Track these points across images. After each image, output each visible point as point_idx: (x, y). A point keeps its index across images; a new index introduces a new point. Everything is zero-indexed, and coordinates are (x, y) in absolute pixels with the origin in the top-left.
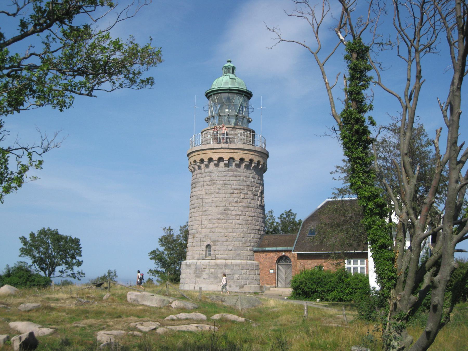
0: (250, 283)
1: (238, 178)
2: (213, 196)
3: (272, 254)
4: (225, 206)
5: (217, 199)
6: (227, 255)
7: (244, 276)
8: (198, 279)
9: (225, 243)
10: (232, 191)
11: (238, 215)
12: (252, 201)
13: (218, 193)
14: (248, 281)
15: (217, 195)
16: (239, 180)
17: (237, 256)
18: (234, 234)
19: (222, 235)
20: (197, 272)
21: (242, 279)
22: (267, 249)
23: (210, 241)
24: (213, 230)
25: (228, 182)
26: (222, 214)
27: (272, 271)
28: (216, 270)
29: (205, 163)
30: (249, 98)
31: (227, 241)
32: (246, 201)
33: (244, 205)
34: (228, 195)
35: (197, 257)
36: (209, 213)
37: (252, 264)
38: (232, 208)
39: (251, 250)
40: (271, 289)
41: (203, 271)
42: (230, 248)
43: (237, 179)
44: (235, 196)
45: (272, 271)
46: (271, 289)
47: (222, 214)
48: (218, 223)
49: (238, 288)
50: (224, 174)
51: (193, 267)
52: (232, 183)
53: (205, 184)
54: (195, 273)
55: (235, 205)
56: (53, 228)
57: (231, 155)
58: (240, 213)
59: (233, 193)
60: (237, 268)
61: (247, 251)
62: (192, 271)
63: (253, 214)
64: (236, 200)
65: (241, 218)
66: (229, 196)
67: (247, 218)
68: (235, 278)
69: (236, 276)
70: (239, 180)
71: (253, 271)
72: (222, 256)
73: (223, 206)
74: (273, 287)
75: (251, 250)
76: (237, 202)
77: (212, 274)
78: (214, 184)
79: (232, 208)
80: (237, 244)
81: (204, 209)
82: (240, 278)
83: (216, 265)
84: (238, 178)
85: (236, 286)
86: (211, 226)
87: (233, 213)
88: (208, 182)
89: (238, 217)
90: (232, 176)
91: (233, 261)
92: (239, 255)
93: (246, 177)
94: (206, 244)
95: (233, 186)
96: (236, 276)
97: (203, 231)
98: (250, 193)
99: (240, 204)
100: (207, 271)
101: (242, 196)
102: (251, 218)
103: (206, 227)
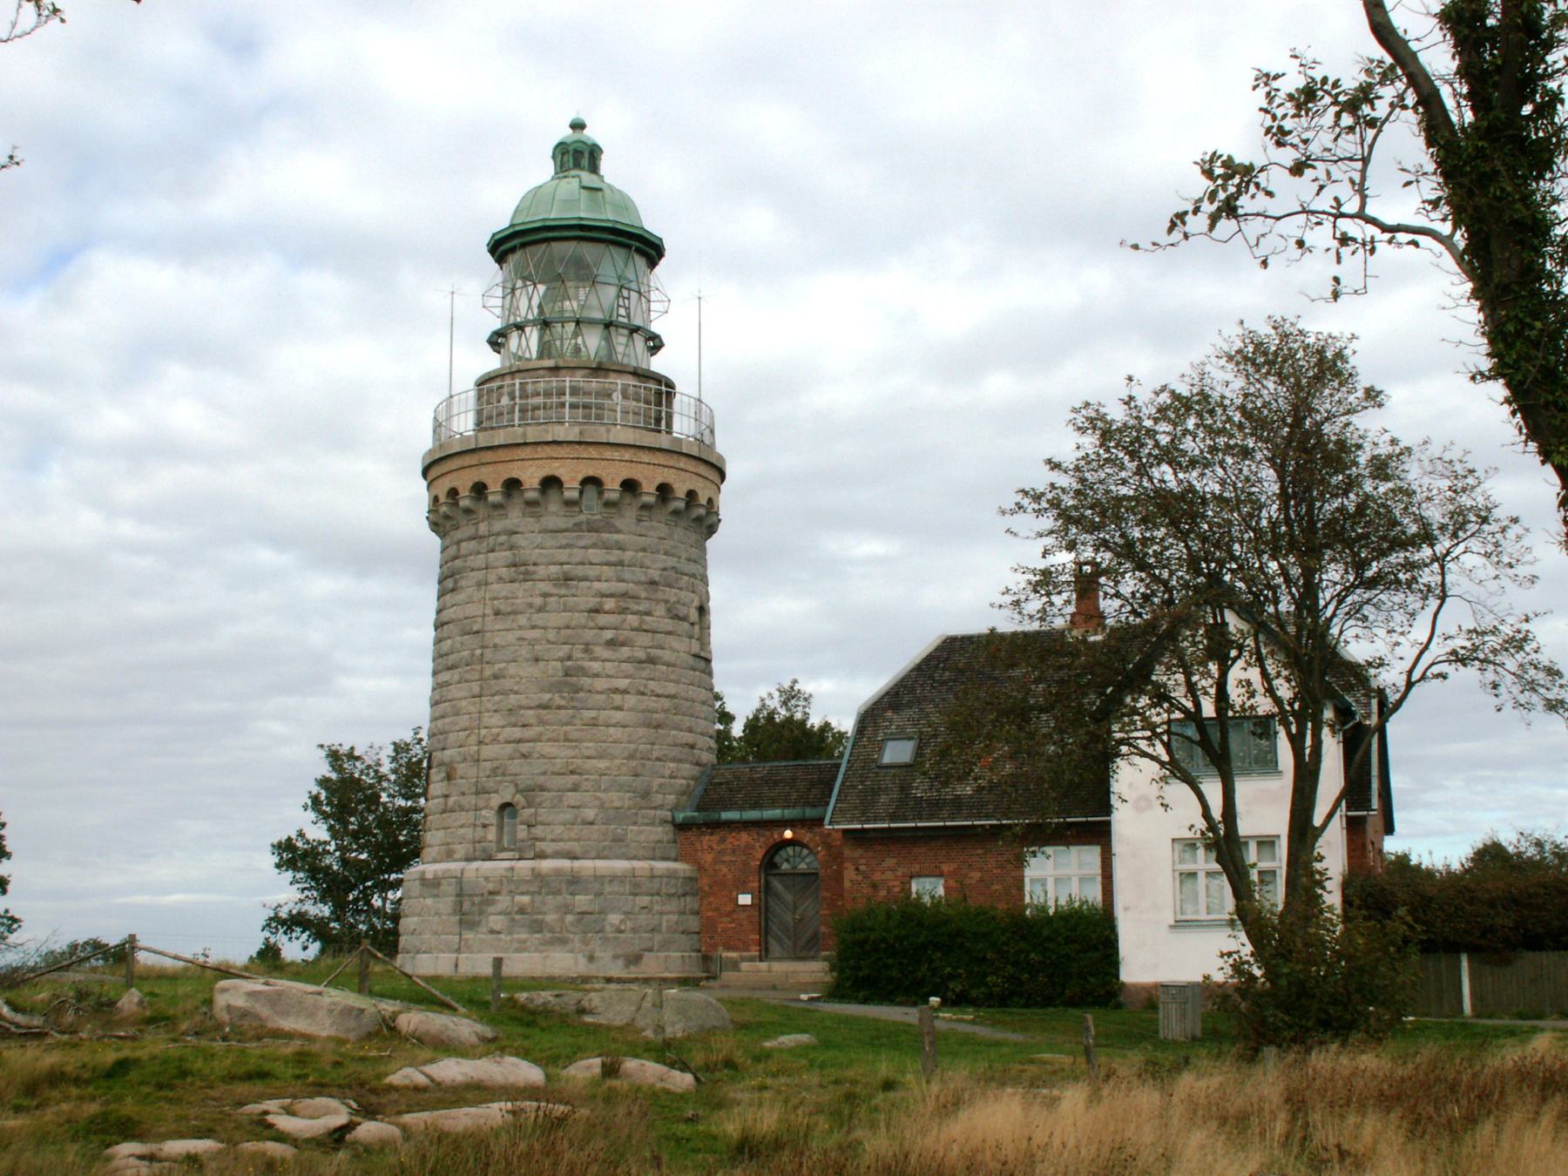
0: (665, 946)
1: (615, 555)
3: (745, 837)
4: (569, 658)
6: (578, 840)
7: (643, 919)
8: (468, 935)
9: (572, 798)
10: (593, 602)
11: (616, 691)
12: (670, 638)
13: (541, 610)
14: (658, 938)
15: (539, 619)
16: (621, 563)
17: (616, 846)
19: (555, 769)
20: (466, 906)
21: (634, 930)
22: (726, 815)
23: (512, 789)
24: (524, 747)
25: (580, 571)
26: (556, 687)
27: (745, 899)
28: (538, 898)
29: (491, 498)
30: (652, 263)
31: (575, 788)
32: (644, 639)
33: (641, 655)
34: (581, 618)
35: (461, 850)
36: (507, 684)
37: (672, 875)
38: (596, 666)
40: (744, 966)
42: (590, 814)
43: (613, 559)
44: (602, 619)
45: (745, 899)
46: (744, 966)
47: (556, 687)
48: (542, 722)
49: (620, 962)
50: (563, 539)
51: (448, 888)
52: (592, 572)
53: (492, 577)
54: (458, 909)
55: (606, 654)
57: (626, 472)
58: (623, 683)
59: (597, 611)
60: (616, 887)
61: (652, 824)
62: (446, 904)
63: (672, 688)
64: (609, 634)
66: (583, 621)
67: (652, 703)
68: (608, 928)
69: (614, 918)
70: (621, 563)
72: (561, 846)
73: (562, 660)
74: (751, 959)
76: (611, 643)
78: (527, 577)
79: (596, 666)
80: (615, 798)
81: (488, 672)
82: (629, 924)
83: (537, 876)
84: (615, 555)
85: (615, 957)
87: (601, 684)
88: (504, 571)
89: (617, 698)
90: (594, 546)
91: (600, 864)
92: (618, 840)
93: (644, 550)
94: (496, 801)
95: (596, 585)
96: (614, 918)
97: (487, 751)
98: (660, 610)
99: (625, 652)
100: (503, 901)
101: (633, 620)
102: (666, 703)
103: (495, 740)
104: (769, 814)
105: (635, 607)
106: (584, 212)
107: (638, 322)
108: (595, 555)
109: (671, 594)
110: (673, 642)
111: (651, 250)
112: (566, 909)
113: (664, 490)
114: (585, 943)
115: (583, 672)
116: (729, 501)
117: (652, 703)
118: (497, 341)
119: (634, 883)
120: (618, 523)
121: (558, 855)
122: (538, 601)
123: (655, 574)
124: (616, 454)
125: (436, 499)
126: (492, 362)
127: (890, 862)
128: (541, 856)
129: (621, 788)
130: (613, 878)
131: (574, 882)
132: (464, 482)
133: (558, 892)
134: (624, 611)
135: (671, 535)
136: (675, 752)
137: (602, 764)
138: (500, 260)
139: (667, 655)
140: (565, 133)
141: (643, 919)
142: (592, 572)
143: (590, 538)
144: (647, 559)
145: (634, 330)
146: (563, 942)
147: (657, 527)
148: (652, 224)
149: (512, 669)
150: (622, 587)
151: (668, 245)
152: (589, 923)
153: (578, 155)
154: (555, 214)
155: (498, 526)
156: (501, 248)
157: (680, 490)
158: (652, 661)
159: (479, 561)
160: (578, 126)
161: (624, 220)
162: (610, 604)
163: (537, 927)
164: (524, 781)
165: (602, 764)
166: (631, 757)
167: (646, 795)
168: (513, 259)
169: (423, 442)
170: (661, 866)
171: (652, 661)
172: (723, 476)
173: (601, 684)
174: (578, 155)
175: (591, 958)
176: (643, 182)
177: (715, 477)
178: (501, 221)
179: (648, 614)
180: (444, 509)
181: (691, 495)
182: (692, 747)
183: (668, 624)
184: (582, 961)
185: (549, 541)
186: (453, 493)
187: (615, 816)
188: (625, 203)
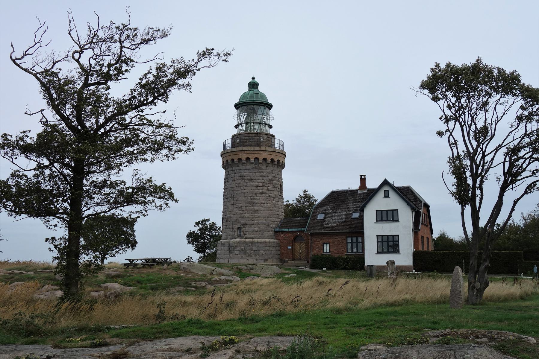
0: (272, 257)
2: (242, 188)
7: (268, 251)
8: (231, 255)
11: (262, 203)
17: (262, 236)
22: (285, 230)
24: (243, 215)
27: (289, 248)
30: (270, 109)
32: (267, 192)
33: (267, 195)
34: (255, 188)
35: (229, 237)
36: (239, 202)
37: (274, 242)
40: (289, 262)
41: (235, 248)
42: (256, 229)
44: (259, 188)
45: (289, 248)
46: (289, 262)
47: (249, 202)
48: (246, 210)
49: (263, 261)
51: (227, 245)
52: (257, 178)
55: (260, 195)
57: (264, 156)
64: (261, 191)
69: (262, 251)
72: (250, 236)
76: (261, 193)
77: (242, 250)
78: (243, 179)
79: (258, 198)
88: (238, 178)
91: (258, 240)
100: (238, 248)
102: (273, 206)
103: (236, 214)
104: (294, 230)
107: (267, 123)
108: (258, 174)
111: (270, 106)
114: (256, 256)
115: (255, 199)
116: (287, 161)
118: (236, 127)
120: (262, 167)
123: (270, 178)
126: (235, 132)
127: (319, 240)
128: (246, 238)
129: (263, 224)
130: (261, 243)
132: (229, 159)
134: (263, 186)
137: (259, 219)
141: (268, 251)
142: (257, 178)
143: (257, 170)
146: (251, 256)
147: (270, 168)
148: (270, 101)
149: (240, 199)
150: (263, 181)
153: (253, 85)
155: (237, 168)
156: (237, 106)
157: (276, 160)
158: (269, 196)
159: (233, 175)
160: (253, 78)
162: (261, 185)
163: (245, 253)
165: (259, 219)
171: (269, 196)
173: (259, 202)
174: (253, 85)
175: (257, 260)
177: (284, 156)
181: (278, 161)
184: (255, 260)
186: (227, 161)
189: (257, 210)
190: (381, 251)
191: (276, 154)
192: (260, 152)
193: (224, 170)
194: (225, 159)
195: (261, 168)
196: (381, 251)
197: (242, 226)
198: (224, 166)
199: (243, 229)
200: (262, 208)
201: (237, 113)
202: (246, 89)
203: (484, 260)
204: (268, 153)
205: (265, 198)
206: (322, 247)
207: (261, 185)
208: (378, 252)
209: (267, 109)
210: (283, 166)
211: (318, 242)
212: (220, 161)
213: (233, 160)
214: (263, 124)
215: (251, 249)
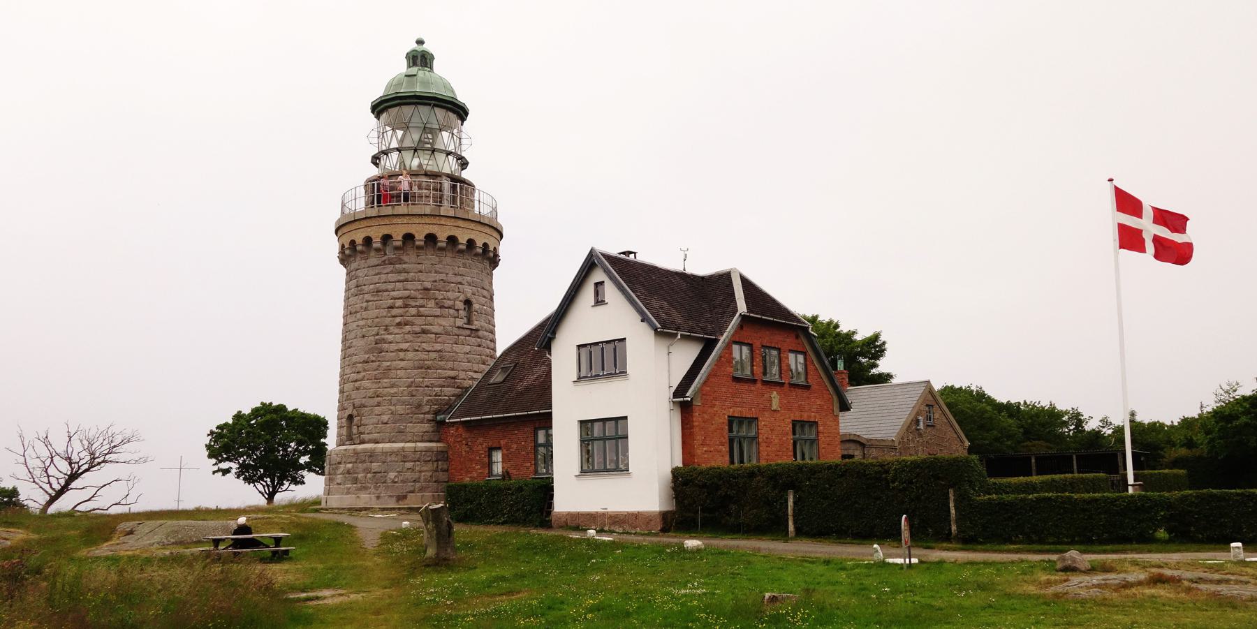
0: (422, 490)
1: (403, 276)
2: (358, 315)
5: (362, 323)
7: (409, 475)
9: (377, 410)
10: (390, 302)
11: (401, 350)
13: (366, 309)
14: (418, 485)
15: (365, 314)
16: (406, 280)
17: (400, 435)
18: (395, 390)
21: (403, 481)
25: (383, 286)
26: (370, 351)
29: (375, 245)
30: (463, 119)
31: (378, 405)
32: (419, 321)
33: (418, 329)
34: (384, 312)
37: (429, 450)
38: (390, 337)
39: (429, 421)
42: (385, 418)
44: (394, 312)
47: (370, 351)
50: (377, 270)
52: (390, 286)
55: (397, 331)
56: (824, 318)
57: (385, 231)
58: (405, 346)
61: (422, 422)
63: (438, 347)
64: (398, 320)
65: (410, 355)
67: (422, 355)
69: (392, 475)
70: (406, 280)
71: (430, 465)
72: (371, 436)
75: (429, 421)
76: (399, 324)
77: (348, 472)
79: (390, 337)
83: (356, 453)
84: (403, 276)
85: (845, 407)
86: (354, 376)
87: (393, 347)
90: (392, 272)
91: (388, 445)
96: (392, 475)
99: (408, 328)
101: (413, 311)
102: (434, 355)
105: (414, 304)
106: (419, 89)
108: (392, 277)
109: (439, 295)
110: (441, 321)
111: (461, 112)
112: (367, 471)
113: (471, 243)
114: (376, 488)
115: (384, 341)
116: (504, 250)
117: (422, 355)
118: (376, 160)
119: (403, 456)
120: (405, 258)
121: (370, 441)
122: (364, 305)
123: (428, 285)
124: (399, 221)
125: (343, 246)
126: (374, 171)
127: (481, 440)
128: (362, 442)
129: (403, 403)
130: (392, 453)
131: (372, 455)
132: (359, 237)
133: (364, 462)
134: (406, 306)
135: (440, 262)
136: (440, 382)
137: (393, 391)
138: (378, 117)
139: (435, 329)
140: (414, 46)
141: (409, 475)
142: (390, 286)
143: (390, 268)
144: (422, 276)
145: (449, 153)
146: (366, 488)
147: (429, 258)
148: (461, 98)
150: (407, 293)
151: (469, 106)
152: (379, 478)
153: (421, 59)
154: (404, 90)
156: (378, 108)
157: (479, 243)
158: (424, 332)
161: (443, 93)
162: (399, 303)
163: (356, 481)
164: (357, 402)
165: (393, 391)
166: (409, 386)
167: (419, 406)
168: (384, 115)
169: (335, 216)
170: (421, 445)
171: (424, 332)
172: (501, 237)
173: (393, 347)
174: (421, 59)
175: (378, 497)
176: (450, 73)
177: (496, 235)
178: (378, 93)
179: (423, 306)
180: (347, 252)
181: (485, 245)
182: (454, 378)
183: (438, 311)
184: (374, 499)
185: (372, 271)
186: (353, 243)
187: (399, 418)
188: (447, 86)
189: (389, 369)
190: (619, 467)
191: (443, 221)
192: (396, 220)
193: (343, 271)
194: (346, 240)
195: (401, 261)
196: (619, 467)
197: (355, 413)
198: (344, 259)
199: (356, 419)
200: (402, 364)
201: (464, 147)
202: (402, 67)
203: (389, 551)
204: (417, 220)
205: (409, 337)
206: (486, 460)
207: (399, 303)
208: (583, 472)
209: (452, 116)
210: (494, 261)
211: (481, 445)
212: (333, 246)
213: (353, 243)
214: (441, 151)
215: (367, 471)
